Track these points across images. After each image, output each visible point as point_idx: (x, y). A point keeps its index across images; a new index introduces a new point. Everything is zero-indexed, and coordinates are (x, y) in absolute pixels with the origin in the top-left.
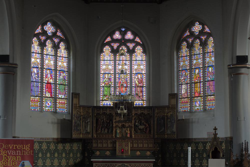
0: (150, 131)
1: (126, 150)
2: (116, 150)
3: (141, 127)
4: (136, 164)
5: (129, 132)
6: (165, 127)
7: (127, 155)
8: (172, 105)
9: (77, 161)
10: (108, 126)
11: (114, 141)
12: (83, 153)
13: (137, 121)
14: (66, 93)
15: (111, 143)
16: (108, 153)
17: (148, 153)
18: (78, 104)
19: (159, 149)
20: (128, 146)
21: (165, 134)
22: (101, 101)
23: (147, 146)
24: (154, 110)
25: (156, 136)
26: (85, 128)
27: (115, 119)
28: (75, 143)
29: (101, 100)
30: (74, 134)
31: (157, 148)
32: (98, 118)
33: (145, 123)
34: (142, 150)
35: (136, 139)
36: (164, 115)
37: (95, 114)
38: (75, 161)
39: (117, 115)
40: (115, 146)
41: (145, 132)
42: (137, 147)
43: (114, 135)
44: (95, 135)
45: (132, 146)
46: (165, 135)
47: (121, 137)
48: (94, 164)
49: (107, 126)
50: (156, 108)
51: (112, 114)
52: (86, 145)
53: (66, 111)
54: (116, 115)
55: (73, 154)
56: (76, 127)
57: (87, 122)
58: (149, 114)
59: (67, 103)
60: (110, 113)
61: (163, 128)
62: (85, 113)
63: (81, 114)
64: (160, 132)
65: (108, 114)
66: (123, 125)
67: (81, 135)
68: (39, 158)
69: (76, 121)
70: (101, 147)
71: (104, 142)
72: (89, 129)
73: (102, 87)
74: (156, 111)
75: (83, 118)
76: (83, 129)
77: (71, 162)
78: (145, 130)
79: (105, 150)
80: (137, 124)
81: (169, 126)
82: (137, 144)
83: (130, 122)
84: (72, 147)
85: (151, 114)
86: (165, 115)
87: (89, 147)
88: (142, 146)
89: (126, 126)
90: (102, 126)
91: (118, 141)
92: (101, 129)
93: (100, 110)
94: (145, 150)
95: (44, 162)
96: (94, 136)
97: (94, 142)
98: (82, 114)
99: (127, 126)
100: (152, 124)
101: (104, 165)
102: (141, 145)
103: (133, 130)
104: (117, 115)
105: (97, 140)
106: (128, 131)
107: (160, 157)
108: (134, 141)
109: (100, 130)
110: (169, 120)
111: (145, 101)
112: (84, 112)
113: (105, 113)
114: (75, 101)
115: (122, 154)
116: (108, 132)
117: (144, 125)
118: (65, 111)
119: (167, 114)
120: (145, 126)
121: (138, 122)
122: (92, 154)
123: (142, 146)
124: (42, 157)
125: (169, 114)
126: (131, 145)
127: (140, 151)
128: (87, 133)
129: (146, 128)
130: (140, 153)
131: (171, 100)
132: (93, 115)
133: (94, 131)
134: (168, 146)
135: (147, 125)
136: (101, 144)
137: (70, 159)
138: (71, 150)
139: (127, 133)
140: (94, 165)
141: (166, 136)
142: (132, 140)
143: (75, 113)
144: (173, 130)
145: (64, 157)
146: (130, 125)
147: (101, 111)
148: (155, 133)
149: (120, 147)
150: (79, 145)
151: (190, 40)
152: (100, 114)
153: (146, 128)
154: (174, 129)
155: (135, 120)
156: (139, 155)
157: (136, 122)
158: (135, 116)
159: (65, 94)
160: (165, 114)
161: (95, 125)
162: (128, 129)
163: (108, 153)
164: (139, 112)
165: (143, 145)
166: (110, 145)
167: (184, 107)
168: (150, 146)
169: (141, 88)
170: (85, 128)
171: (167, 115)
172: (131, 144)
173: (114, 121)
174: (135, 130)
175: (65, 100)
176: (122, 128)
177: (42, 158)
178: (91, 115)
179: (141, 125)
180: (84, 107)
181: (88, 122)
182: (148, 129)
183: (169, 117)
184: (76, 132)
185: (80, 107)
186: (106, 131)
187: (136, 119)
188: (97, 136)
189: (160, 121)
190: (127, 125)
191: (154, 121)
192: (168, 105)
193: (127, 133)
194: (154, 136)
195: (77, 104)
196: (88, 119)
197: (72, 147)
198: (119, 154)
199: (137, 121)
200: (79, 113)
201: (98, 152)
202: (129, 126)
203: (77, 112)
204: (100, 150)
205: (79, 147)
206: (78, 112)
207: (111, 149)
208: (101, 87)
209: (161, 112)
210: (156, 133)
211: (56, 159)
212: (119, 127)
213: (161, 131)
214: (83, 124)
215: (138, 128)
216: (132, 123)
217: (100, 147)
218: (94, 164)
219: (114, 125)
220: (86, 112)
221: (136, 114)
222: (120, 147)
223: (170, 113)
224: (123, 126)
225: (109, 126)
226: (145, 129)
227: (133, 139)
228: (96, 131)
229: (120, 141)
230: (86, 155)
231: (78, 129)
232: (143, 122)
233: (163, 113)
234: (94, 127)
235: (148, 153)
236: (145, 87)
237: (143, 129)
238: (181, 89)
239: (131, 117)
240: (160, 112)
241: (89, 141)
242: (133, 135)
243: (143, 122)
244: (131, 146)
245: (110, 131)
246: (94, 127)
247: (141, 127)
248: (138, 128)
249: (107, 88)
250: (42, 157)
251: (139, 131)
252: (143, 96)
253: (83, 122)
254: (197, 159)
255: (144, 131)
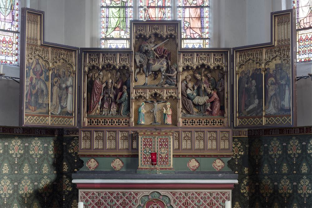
0: (222, 109)
1: (163, 155)
2: (137, 156)
3: (201, 100)
4: (189, 192)
5: (170, 112)
6: (260, 98)
7: (166, 169)
8: (279, 41)
9: (41, 185)
10: (119, 97)
11: (132, 134)
12: (57, 165)
13: (190, 85)
14: (16, 18)
15: (125, 138)
16: (118, 164)
17: (219, 164)
18: (38, 38)
19: (243, 153)
20: (166, 145)
21: (262, 115)
22: (103, 41)
23: (214, 147)
24: (232, 57)
25: (237, 122)
26: (60, 102)
27: (136, 81)
28: (36, 139)
29: (103, 39)
30: (27, 116)
31: (240, 151)
32: (94, 79)
33: (209, 91)
34: (204, 156)
35: (189, 130)
36: (258, 67)
37: (87, 69)
38: (36, 184)
39: (140, 70)
40: (135, 146)
41: (211, 113)
42: (191, 149)
43: (133, 119)
44: (86, 120)
45: (177, 147)
46: (261, 117)
47: (151, 124)
48: (81, 192)
49: (116, 97)
50: (236, 51)
51: (128, 68)
52: (64, 144)
53: (16, 63)
54: (138, 70)
55: (31, 166)
56: (33, 98)
57: (64, 86)
58: (218, 67)
59: (17, 44)
60: (124, 67)
61: (257, 101)
62: (58, 63)
63: (49, 64)
64: (247, 110)
65: (118, 67)
66: (156, 94)
67: (49, 119)
68: (2, 176)
69: (34, 81)
70: (101, 149)
71: (107, 136)
72: (69, 106)
73: (105, 7)
74: (238, 59)
75: (55, 75)
76: (54, 102)
77: (27, 187)
78: (209, 108)
79: (109, 156)
80: (189, 92)
81: (271, 93)
82: (189, 142)
83: (174, 86)
84: (27, 150)
85: (224, 68)
86: (260, 69)
87: (73, 149)
88: (202, 147)
89: (162, 98)
90: (104, 96)
91: (142, 133)
92: (102, 106)
93: (99, 58)
94: (210, 156)
95: (15, 185)
96: (84, 123)
97: (82, 136)
98: (51, 64)
99: (165, 98)
100: (227, 93)
101: (106, 194)
102: (199, 145)
103: (181, 106)
104: (140, 70)
105: (90, 132)
106: (166, 109)
107: (246, 172)
108: (183, 135)
109: (99, 107)
110: (273, 79)
111: (207, 41)
112: (56, 62)
113: (109, 65)
114: (32, 30)
115: (152, 167)
116: (118, 111)
117: (208, 95)
118: (13, 63)
119: (265, 65)
120: (210, 98)
121: (193, 88)
122: (77, 164)
123: (202, 147)
124: (49, 175)
125: (272, 65)
126: (175, 145)
127: (197, 159)
128: (66, 114)
129: (212, 103)
130: (197, 164)
131: (276, 27)
132: (80, 70)
133: (84, 110)
134: (266, 145)
135: (215, 96)
136: (101, 142)
137: (23, 178)
138: (26, 157)
139: (165, 114)
140: (80, 195)
141: (264, 119)
142: (178, 132)
143: (31, 61)
144: (284, 105)
145: (5, 174)
146: (173, 95)
147: (101, 59)
148: (236, 115)
149: (148, 149)
150: (46, 145)
151: (288, 83)
152: (98, 68)
153: (212, 103)
154: (287, 103)
155: (185, 82)
156: (195, 168)
157: (187, 87)
158: (186, 74)
159: (13, 20)
160: (260, 65)
161: (85, 95)
162: (168, 104)
163: (118, 164)
164: (195, 62)
165: (205, 145)
166: (123, 145)
167: (305, 51)
168: (222, 146)
169: (198, 10)
170: (60, 102)
171: (267, 67)
172: (176, 143)
173: (133, 84)
174: (184, 107)
175: (10, 34)
176: (152, 102)
177: (270, 176)
178: (75, 69)
179: (198, 95)
180: (56, 48)
181: (67, 88)
182: (217, 105)
183: (271, 72)
184: (35, 111)
185: (46, 45)
186: (114, 109)
187: (188, 80)
188: (90, 122)
189: (247, 84)
190: (165, 95)
191: (232, 86)
192: (269, 41)
193: (165, 114)
194: (232, 121)
195: (36, 40)
196: (67, 80)
197: (27, 150)
198: (144, 167)
199: (190, 85)
200: (44, 63)
201: (93, 160)
202: (171, 97)
203: (38, 60)
204: (97, 156)
205: (46, 150)
206: (40, 61)
207: (126, 154)
208: (103, 7)
209: (251, 61)
210: (237, 114)
211: (6, 177)
212: (145, 100)
213: (251, 107)
214: (54, 91)
215: (193, 104)
216: (178, 88)
217: (97, 149)
218: (80, 190)
219: (133, 96)
220: (62, 61)
221: (188, 67)
222: (148, 149)
223: (274, 62)
224: (156, 97)
225: (120, 97)
226: (209, 104)
227: (180, 130)
228: (89, 110)
229: (146, 133)
230: (66, 168)
231: (40, 101)
232: (204, 88)
233: (255, 63)
234: (84, 99)
235: (219, 164)
236: (207, 7)
237: (205, 104)
238: (298, 8)
239: (174, 74)
240: (246, 62)
241: (72, 135)
242: (180, 120)
243: (204, 88)
244: (176, 147)
245: (123, 109)
246: (84, 99)
247: (201, 100)
248: (193, 104)
249: (118, 9)
250: (30, 175)
251: (195, 110)
252: (202, 28)
253: (53, 86)
254: (6, 177)
255: (208, 110)
